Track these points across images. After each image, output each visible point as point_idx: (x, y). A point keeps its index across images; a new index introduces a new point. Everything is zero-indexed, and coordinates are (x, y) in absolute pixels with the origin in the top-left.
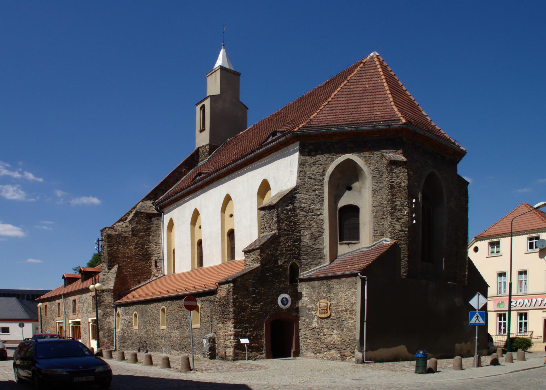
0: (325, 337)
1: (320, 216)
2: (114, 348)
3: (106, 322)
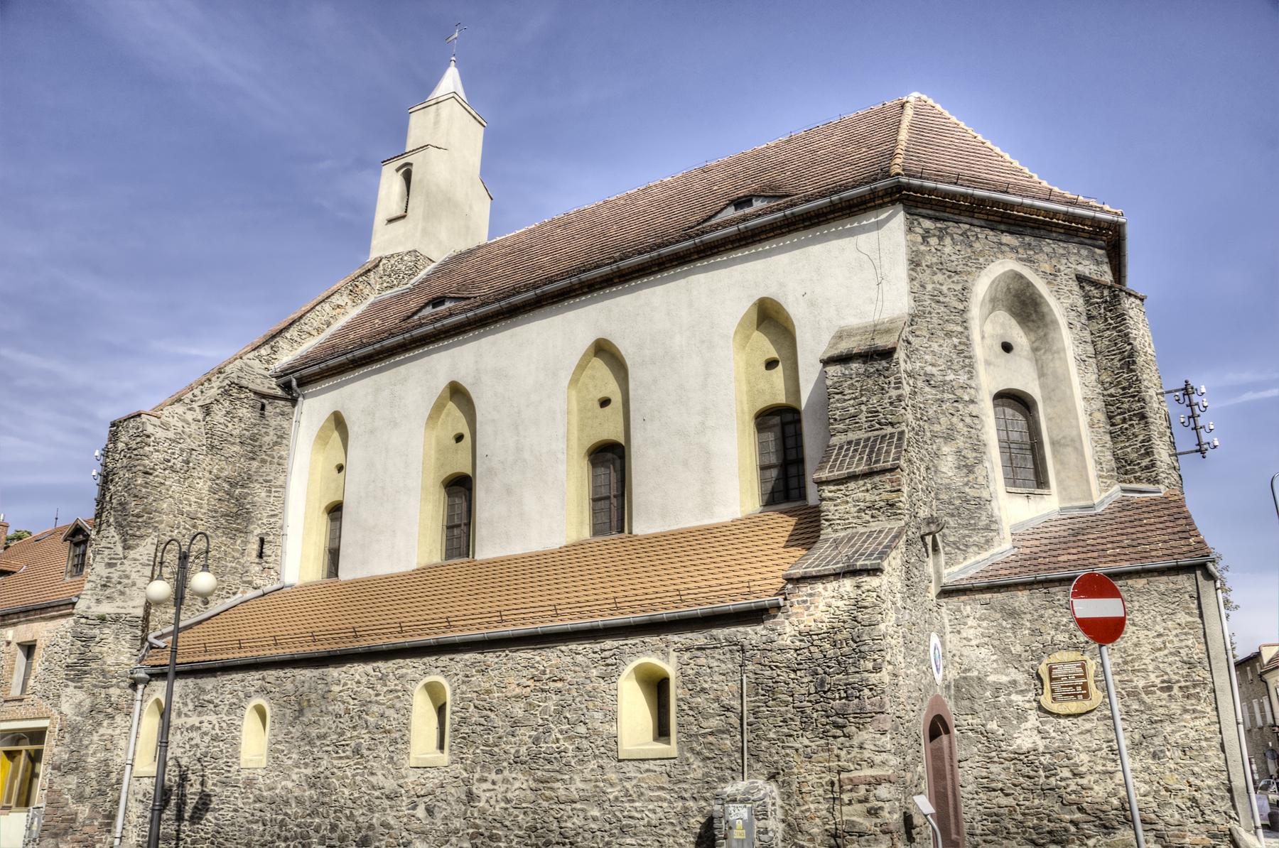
0: (1081, 781)
1: (971, 406)
3: (95, 737)
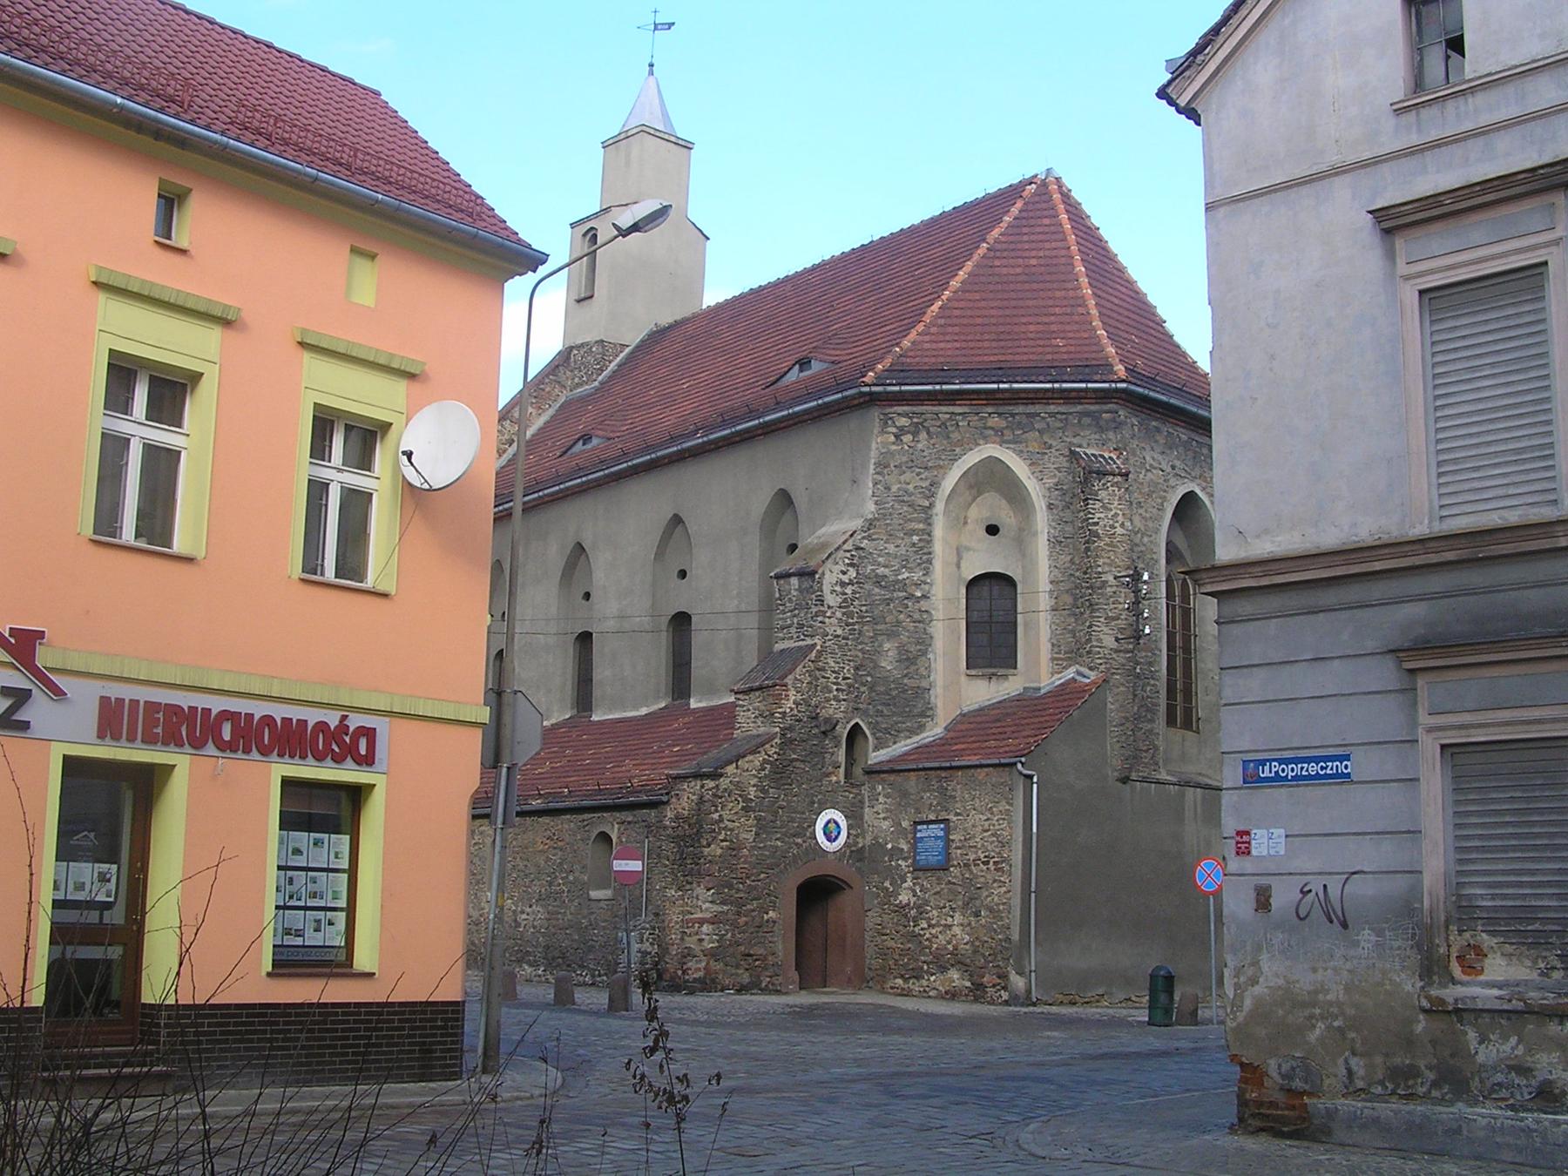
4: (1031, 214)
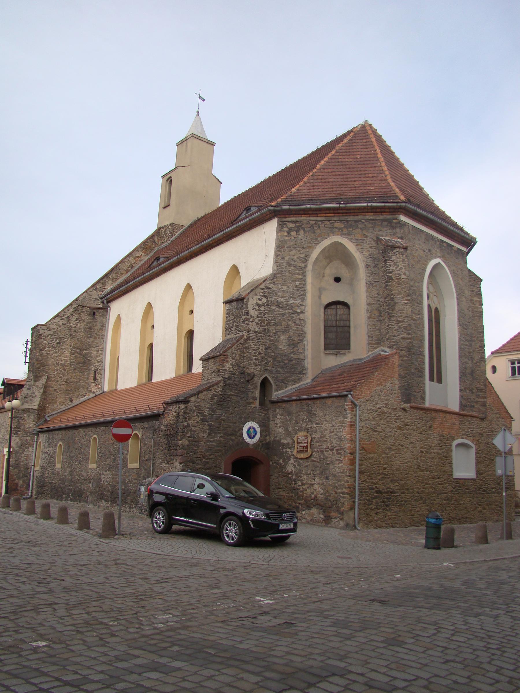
1: (301, 315)
2: (30, 494)
3: (23, 455)
4: (357, 138)
